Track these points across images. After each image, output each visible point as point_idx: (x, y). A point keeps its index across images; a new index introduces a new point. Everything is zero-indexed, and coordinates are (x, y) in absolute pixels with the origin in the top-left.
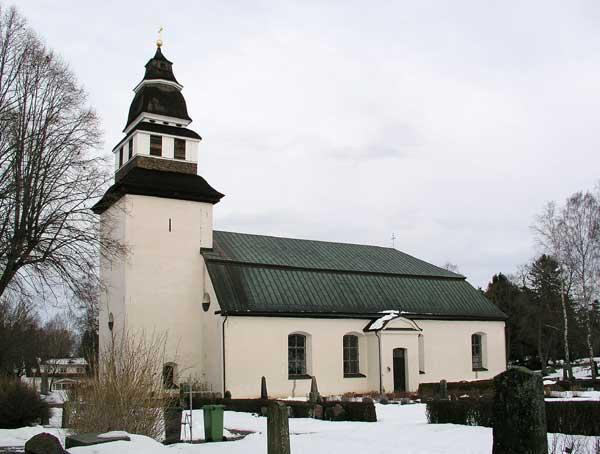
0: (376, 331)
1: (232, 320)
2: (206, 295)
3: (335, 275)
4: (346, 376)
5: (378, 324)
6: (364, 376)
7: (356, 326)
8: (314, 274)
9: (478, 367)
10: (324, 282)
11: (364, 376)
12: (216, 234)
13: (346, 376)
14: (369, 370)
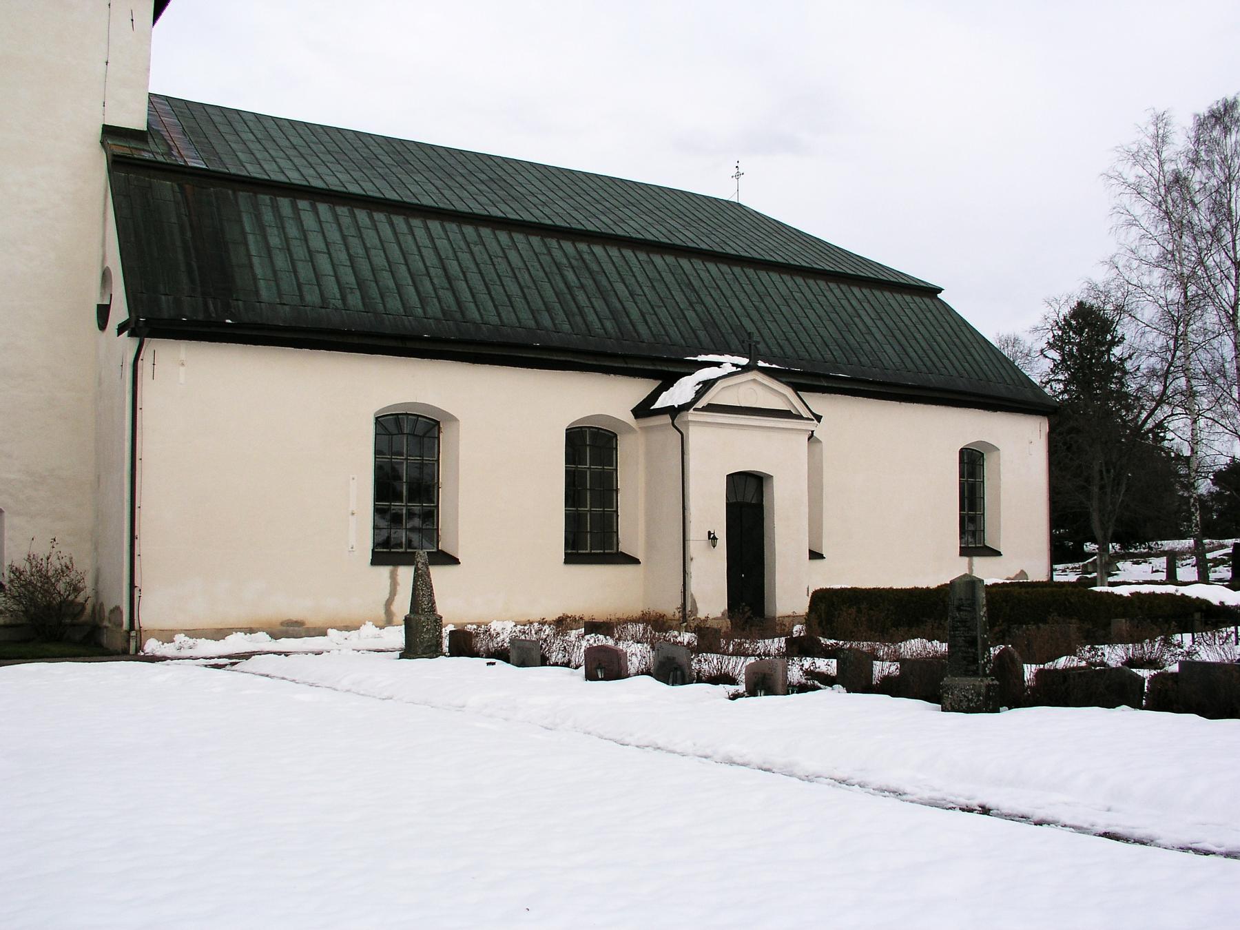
0: (673, 412)
1: (152, 345)
2: (106, 276)
3: (553, 243)
4: (570, 559)
5: (682, 391)
6: (635, 561)
7: (608, 398)
8: (486, 232)
9: (974, 537)
10: (513, 255)
11: (635, 561)
12: (155, 100)
13: (570, 559)
14: (650, 546)
